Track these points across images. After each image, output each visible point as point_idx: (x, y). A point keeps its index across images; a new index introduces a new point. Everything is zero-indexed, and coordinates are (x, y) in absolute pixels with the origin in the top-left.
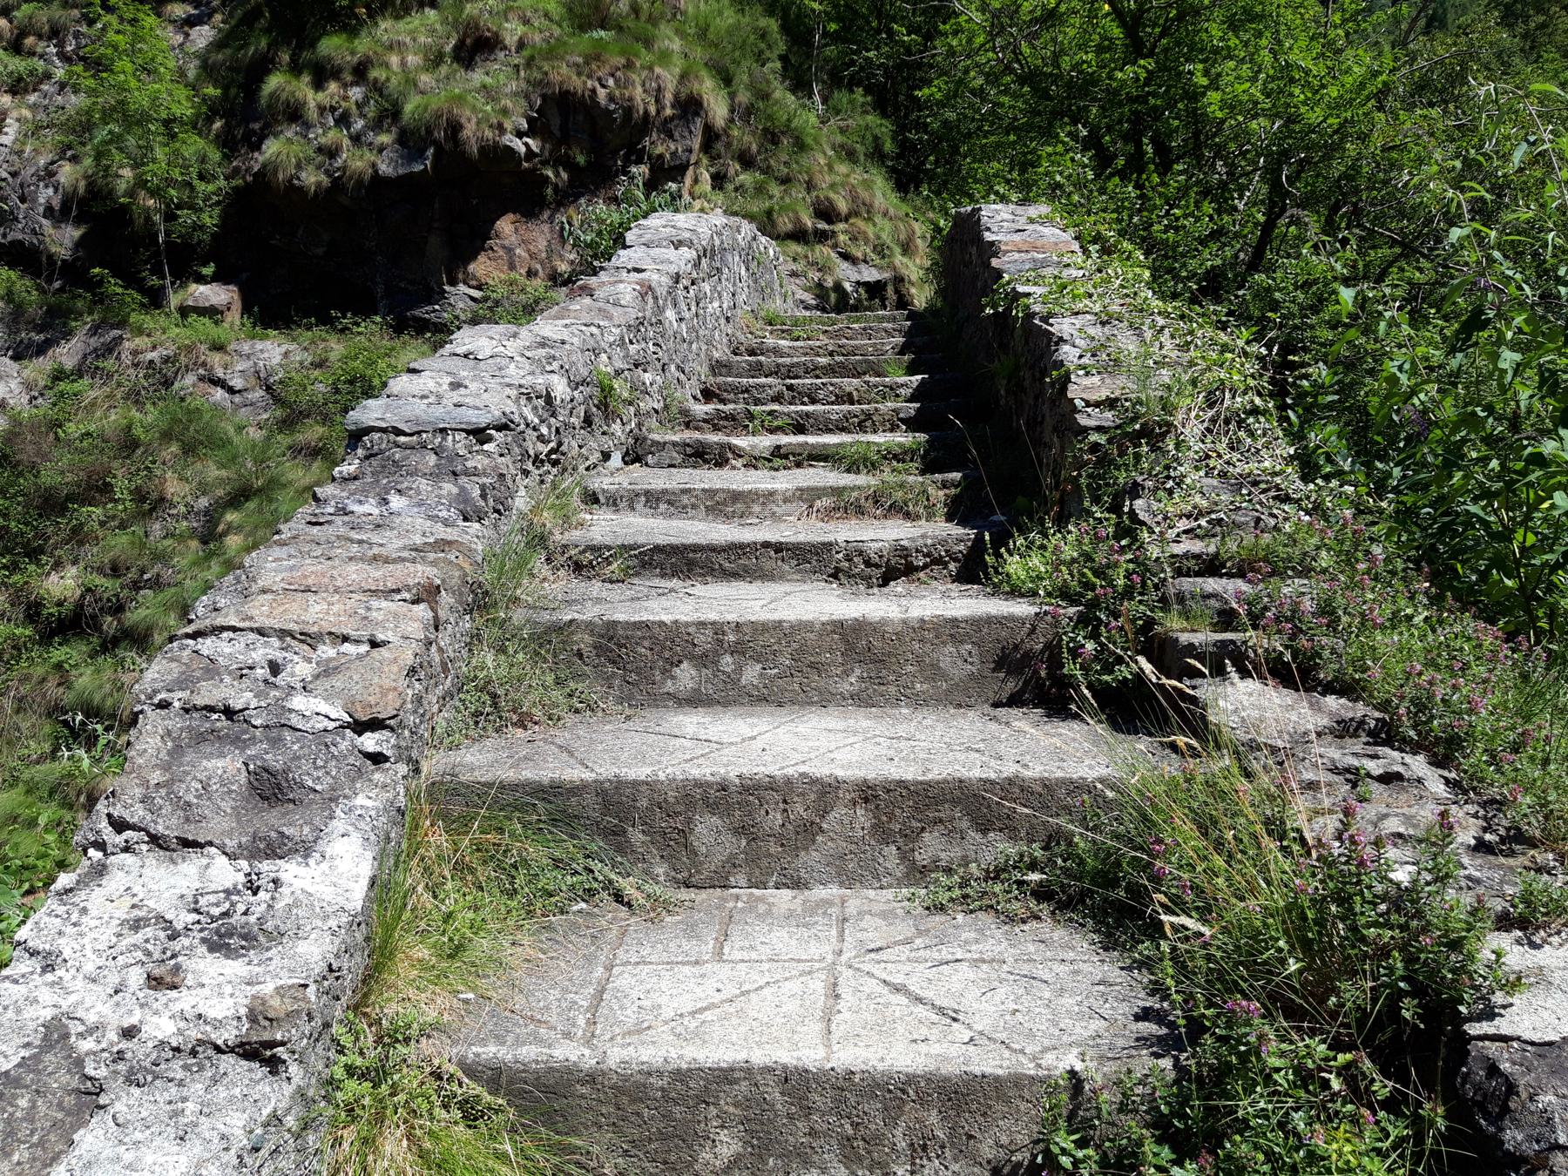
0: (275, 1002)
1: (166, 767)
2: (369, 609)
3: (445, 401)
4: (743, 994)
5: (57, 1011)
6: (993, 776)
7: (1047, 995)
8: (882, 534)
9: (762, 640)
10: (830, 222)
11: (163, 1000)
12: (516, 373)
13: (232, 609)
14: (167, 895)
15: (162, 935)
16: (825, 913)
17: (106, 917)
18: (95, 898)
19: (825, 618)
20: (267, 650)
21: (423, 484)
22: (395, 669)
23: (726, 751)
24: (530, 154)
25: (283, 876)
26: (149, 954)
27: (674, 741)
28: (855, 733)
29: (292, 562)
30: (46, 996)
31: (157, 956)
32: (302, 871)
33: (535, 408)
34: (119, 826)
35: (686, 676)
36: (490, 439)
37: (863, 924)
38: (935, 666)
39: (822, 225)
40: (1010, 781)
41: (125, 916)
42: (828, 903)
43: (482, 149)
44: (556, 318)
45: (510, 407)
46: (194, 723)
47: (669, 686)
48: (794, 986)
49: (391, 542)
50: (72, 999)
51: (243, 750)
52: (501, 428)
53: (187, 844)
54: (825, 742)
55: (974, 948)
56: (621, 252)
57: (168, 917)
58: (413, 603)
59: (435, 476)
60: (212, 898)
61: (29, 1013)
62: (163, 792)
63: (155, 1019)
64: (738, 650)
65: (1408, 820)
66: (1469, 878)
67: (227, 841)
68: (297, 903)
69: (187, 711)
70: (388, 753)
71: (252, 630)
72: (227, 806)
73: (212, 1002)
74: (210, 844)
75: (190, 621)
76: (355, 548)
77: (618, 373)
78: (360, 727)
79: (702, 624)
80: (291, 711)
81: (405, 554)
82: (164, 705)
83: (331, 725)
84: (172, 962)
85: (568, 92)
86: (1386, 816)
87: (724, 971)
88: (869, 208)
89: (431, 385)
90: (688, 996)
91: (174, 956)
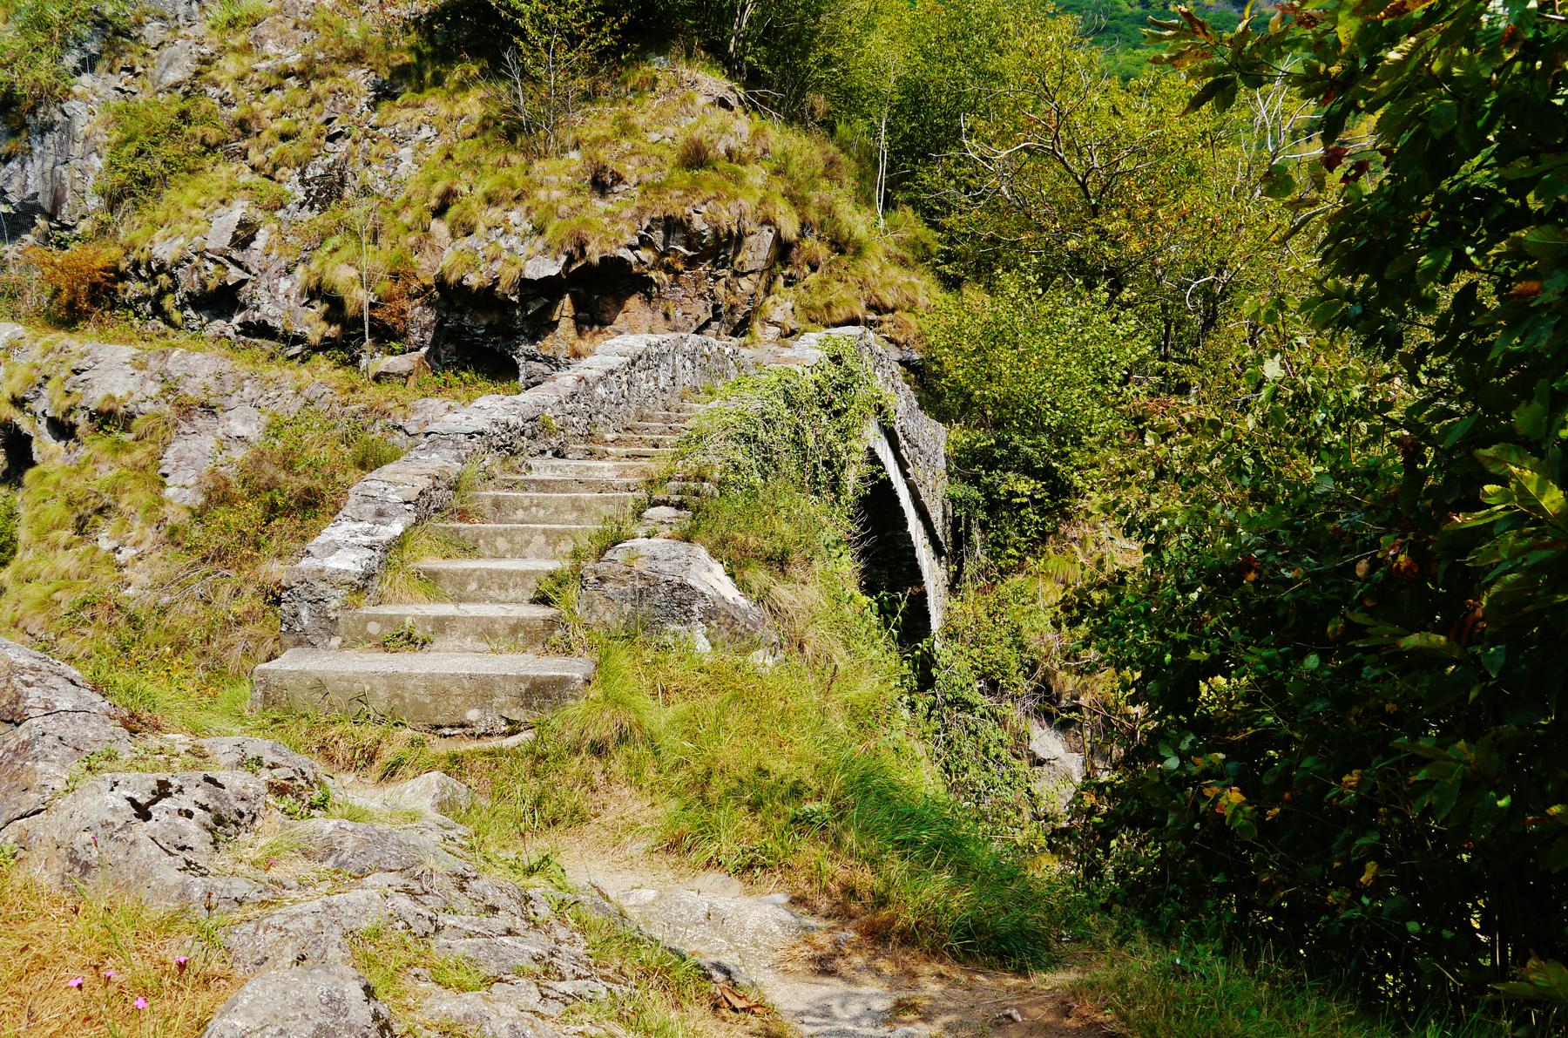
10: (879, 313)
20: (386, 485)
24: (641, 262)
35: (520, 514)
39: (872, 316)
43: (602, 259)
52: (481, 434)
64: (538, 505)
77: (556, 417)
78: (406, 503)
85: (670, 217)
88: (913, 303)
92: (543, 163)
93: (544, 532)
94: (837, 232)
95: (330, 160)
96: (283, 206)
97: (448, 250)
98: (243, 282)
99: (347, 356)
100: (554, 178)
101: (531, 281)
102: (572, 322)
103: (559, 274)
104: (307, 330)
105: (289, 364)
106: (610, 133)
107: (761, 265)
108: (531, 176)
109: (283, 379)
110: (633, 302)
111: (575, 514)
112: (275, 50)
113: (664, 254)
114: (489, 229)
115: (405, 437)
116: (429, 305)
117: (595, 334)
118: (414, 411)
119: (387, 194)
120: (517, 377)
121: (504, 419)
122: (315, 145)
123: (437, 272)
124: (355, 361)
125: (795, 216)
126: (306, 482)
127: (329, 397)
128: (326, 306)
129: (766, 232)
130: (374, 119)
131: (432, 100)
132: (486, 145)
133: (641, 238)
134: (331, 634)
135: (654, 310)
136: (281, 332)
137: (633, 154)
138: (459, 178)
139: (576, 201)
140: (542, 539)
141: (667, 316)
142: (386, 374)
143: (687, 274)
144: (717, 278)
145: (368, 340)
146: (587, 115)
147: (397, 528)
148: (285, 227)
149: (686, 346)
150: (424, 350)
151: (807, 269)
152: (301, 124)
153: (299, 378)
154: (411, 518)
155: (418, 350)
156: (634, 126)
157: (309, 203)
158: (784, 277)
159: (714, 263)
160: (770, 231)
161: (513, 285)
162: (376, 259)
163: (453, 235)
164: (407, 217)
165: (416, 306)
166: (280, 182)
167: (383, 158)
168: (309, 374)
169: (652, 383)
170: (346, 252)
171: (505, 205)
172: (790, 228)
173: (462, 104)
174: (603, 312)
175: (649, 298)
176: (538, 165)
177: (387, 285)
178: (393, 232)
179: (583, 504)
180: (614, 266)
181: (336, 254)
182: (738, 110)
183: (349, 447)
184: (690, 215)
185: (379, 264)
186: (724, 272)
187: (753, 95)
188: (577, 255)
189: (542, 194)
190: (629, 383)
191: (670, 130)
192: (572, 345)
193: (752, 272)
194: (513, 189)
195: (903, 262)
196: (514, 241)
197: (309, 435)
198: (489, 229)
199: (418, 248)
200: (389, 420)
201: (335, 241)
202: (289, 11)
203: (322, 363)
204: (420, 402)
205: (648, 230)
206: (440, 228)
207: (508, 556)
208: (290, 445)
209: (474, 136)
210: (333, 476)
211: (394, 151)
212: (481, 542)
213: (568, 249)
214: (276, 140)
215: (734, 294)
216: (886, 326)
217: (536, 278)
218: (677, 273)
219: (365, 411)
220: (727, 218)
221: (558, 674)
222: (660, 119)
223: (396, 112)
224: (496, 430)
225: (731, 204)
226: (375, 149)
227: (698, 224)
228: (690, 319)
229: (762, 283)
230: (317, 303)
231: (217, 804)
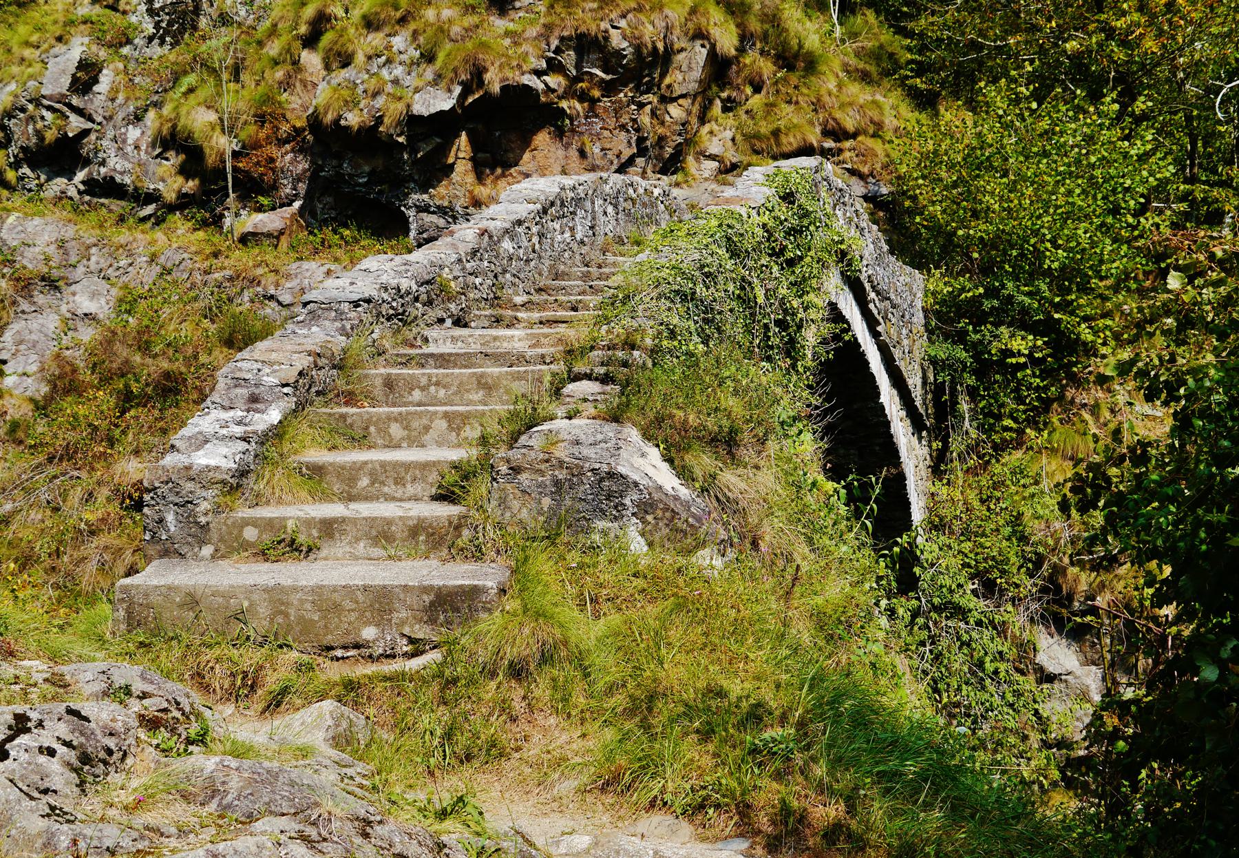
10: (837, 140)
20: (259, 365)
24: (549, 90)
34: (213, 403)
35: (417, 395)
36: (359, 306)
39: (829, 144)
43: (502, 88)
47: (410, 399)
52: (368, 301)
64: (437, 384)
77: (456, 278)
88: (879, 126)
93: (446, 415)
94: (785, 44)
96: (129, 41)
97: (322, 86)
98: (85, 133)
99: (208, 215)
101: (421, 117)
102: (469, 165)
103: (453, 108)
104: (161, 186)
107: (693, 87)
109: (135, 245)
110: (542, 139)
111: (481, 393)
114: (370, 58)
115: (278, 308)
116: (302, 151)
117: (498, 178)
118: (288, 276)
119: (250, 22)
120: (406, 232)
121: (394, 282)
123: (310, 111)
124: (217, 221)
125: (733, 27)
126: (165, 365)
128: (182, 157)
129: (698, 48)
133: (549, 61)
134: (202, 542)
135: (567, 146)
136: (131, 189)
140: (443, 424)
141: (582, 154)
142: (254, 234)
143: (606, 102)
144: (641, 106)
145: (232, 195)
147: (274, 415)
149: (607, 189)
151: (749, 90)
153: (152, 243)
154: (290, 403)
155: (290, 205)
157: (159, 36)
158: (722, 101)
159: (637, 89)
160: (703, 46)
161: (399, 123)
163: (328, 67)
165: (287, 153)
166: (125, 13)
168: (164, 238)
169: (567, 235)
170: (204, 93)
171: (387, 30)
172: (727, 40)
174: (506, 151)
175: (559, 134)
177: (252, 129)
178: (258, 66)
180: (517, 95)
181: (192, 96)
183: (213, 321)
184: (606, 31)
185: (242, 105)
186: (651, 98)
190: (541, 235)
193: (683, 96)
194: (397, 9)
195: (865, 77)
196: (399, 71)
197: (167, 310)
198: (370, 58)
199: (286, 85)
200: (259, 289)
204: (295, 266)
205: (558, 51)
206: (312, 60)
208: (146, 322)
210: (196, 357)
212: (372, 429)
215: (662, 123)
216: (847, 155)
217: (426, 114)
218: (593, 102)
219: (231, 279)
220: (650, 32)
221: (467, 582)
224: (385, 296)
225: (655, 16)
227: (617, 41)
228: (610, 155)
229: (696, 109)
230: (171, 154)
231: (83, 740)
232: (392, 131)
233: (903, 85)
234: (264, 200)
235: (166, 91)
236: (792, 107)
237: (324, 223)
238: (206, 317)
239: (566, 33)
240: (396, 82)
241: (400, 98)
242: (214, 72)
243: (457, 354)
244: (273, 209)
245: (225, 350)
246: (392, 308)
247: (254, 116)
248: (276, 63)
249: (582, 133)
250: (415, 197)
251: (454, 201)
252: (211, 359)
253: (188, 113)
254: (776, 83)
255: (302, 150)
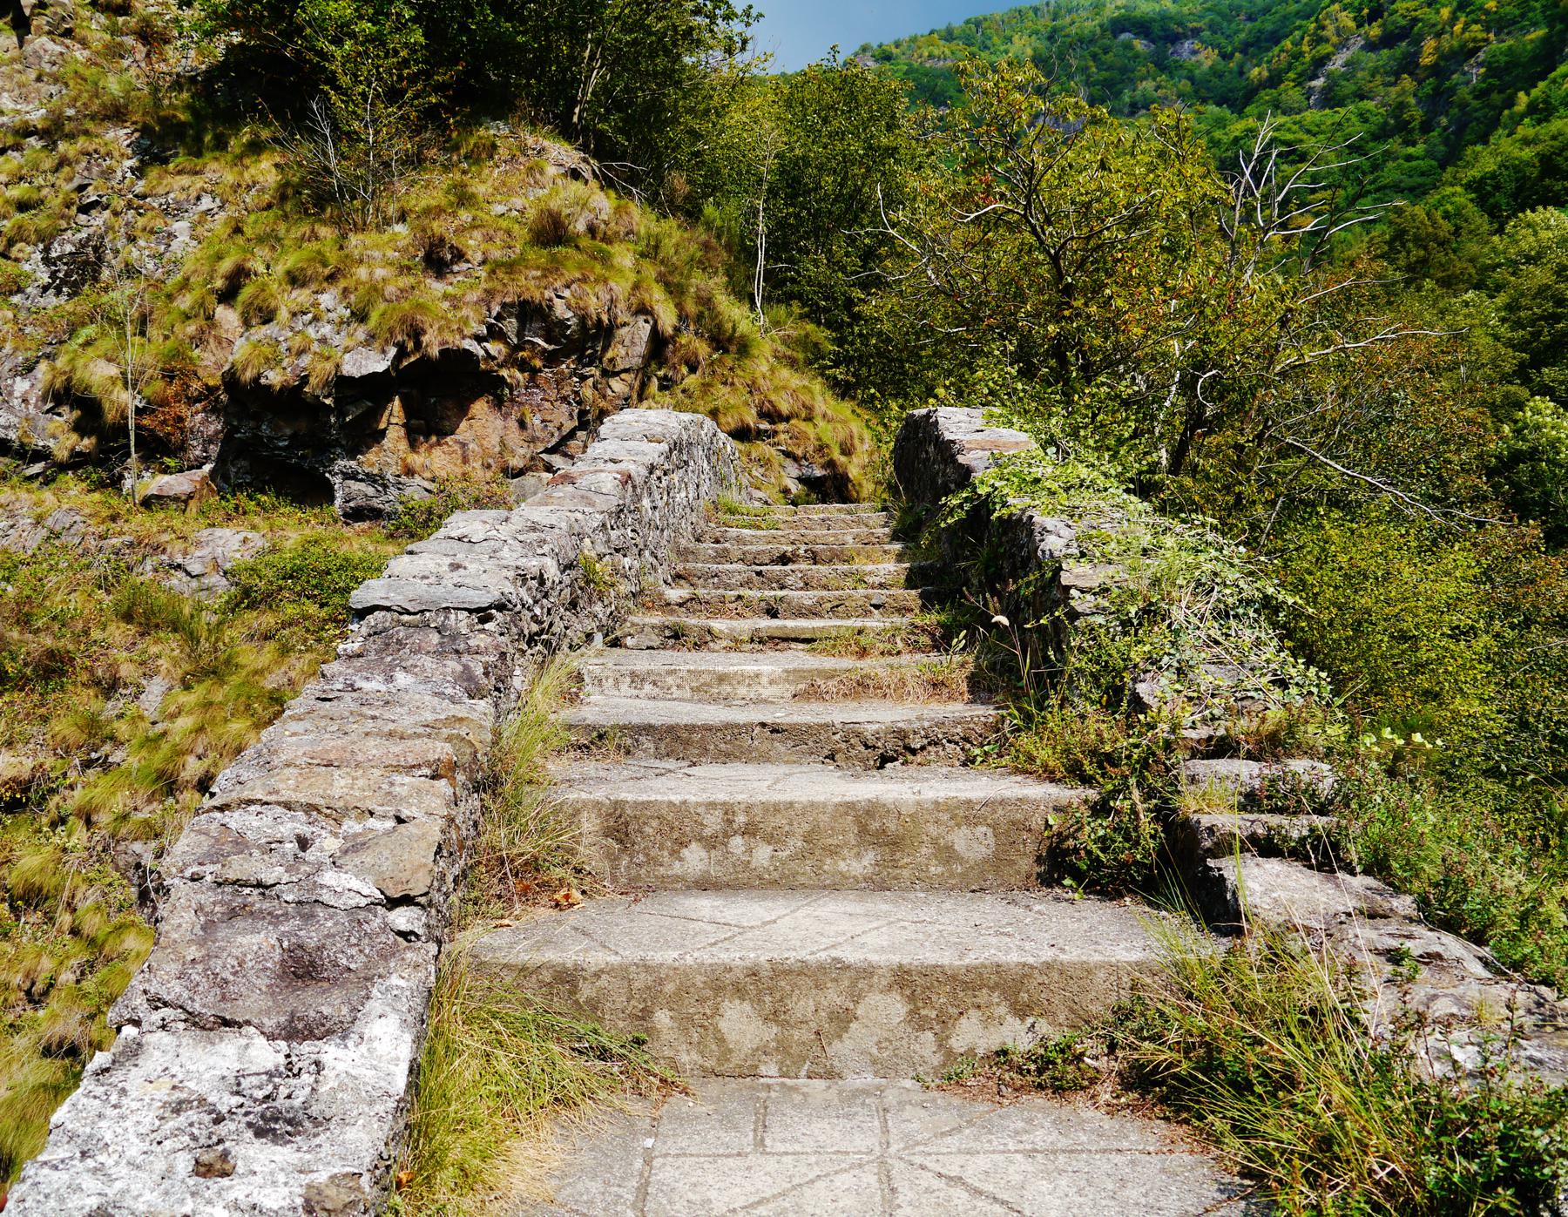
0: (332, 1192)
1: (201, 943)
2: (392, 784)
3: (444, 582)
4: (794, 1188)
5: (103, 1200)
6: (1031, 960)
7: (1110, 1186)
8: (875, 716)
9: (780, 820)
10: (772, 422)
11: (215, 1188)
12: (510, 556)
13: (259, 783)
14: (207, 1076)
15: (207, 1118)
16: (863, 1104)
17: (147, 1099)
18: (133, 1078)
19: (837, 800)
20: (295, 825)
21: (428, 662)
22: (424, 844)
23: (749, 935)
24: (489, 357)
25: (324, 1058)
26: (194, 1138)
27: (692, 925)
28: (878, 917)
29: (312, 736)
30: (90, 1183)
31: (203, 1141)
32: (340, 1053)
33: (529, 589)
34: (156, 1003)
35: (695, 859)
36: (489, 618)
37: (906, 1115)
38: (949, 848)
39: (765, 426)
40: (1048, 966)
41: (166, 1098)
42: (865, 1092)
43: (441, 352)
44: (540, 504)
45: (508, 588)
46: (227, 898)
47: (677, 868)
48: (843, 1181)
49: (406, 722)
50: (118, 1185)
51: (276, 925)
52: (501, 607)
53: (227, 1023)
54: (846, 926)
55: (1024, 1138)
56: (596, 444)
57: (211, 1099)
58: (433, 778)
59: (440, 654)
60: (255, 1080)
61: (74, 1202)
62: (200, 968)
63: (209, 1209)
64: (749, 831)
65: (1458, 1000)
66: (1530, 1058)
67: (265, 1020)
68: (342, 1087)
69: (220, 885)
70: (420, 931)
71: (279, 803)
72: (263, 983)
73: (266, 1191)
74: (248, 1023)
75: (212, 795)
76: (370, 724)
77: (601, 557)
78: (393, 903)
79: (712, 805)
80: (322, 886)
81: (420, 730)
82: (195, 878)
83: (363, 902)
84: (220, 1148)
86: (1435, 997)
87: (771, 1164)
88: (810, 409)
89: (431, 566)
90: (738, 1190)
91: (220, 1141)
92: (360, 236)
94: (719, 326)
95: (83, 235)
96: (20, 290)
97: (239, 342)
99: (104, 475)
100: (376, 254)
101: (351, 379)
102: (402, 432)
103: (387, 371)
104: (51, 443)
105: (26, 485)
106: (444, 202)
107: (637, 362)
108: (346, 251)
109: (17, 505)
110: (480, 407)
111: (869, 857)
112: (11, 105)
113: (519, 348)
114: (294, 314)
115: (186, 579)
116: (214, 411)
117: (432, 446)
118: (198, 544)
119: (158, 274)
120: (331, 500)
122: (63, 217)
123: (226, 368)
124: (115, 483)
125: (672, 305)
126: (48, 642)
127: (81, 528)
128: (77, 413)
129: (641, 323)
130: (140, 187)
131: (214, 165)
132: (286, 217)
133: (490, 327)
135: (506, 417)
136: (16, 445)
137: (476, 227)
138: (253, 253)
139: (406, 281)
140: (895, 1007)
141: (522, 424)
142: (159, 497)
143: (547, 373)
144: (583, 378)
145: (134, 455)
146: (413, 183)
148: (22, 315)
150: (207, 468)
151: (684, 370)
152: (45, 192)
153: (38, 504)
155: (200, 467)
156: (473, 196)
157: (55, 286)
158: (659, 379)
159: (579, 361)
160: (646, 321)
161: (327, 383)
162: (143, 353)
163: (247, 324)
164: (185, 302)
165: (197, 413)
166: (17, 260)
167: (152, 232)
168: (53, 498)
170: (105, 345)
171: (314, 287)
172: (667, 318)
173: (252, 171)
174: (442, 418)
175: (498, 403)
176: (354, 239)
177: (158, 385)
178: (167, 319)
179: (892, 826)
180: (456, 359)
181: (90, 349)
182: (593, 184)
183: (108, 592)
184: (550, 300)
185: (149, 360)
186: (593, 370)
187: (609, 168)
188: (410, 345)
189: (362, 272)
191: (518, 202)
192: (403, 460)
193: (626, 371)
194: (325, 265)
195: (792, 363)
196: (326, 330)
197: (53, 578)
198: (294, 314)
199: (199, 340)
200: (164, 557)
201: (90, 331)
202: (31, 60)
203: (71, 485)
204: (205, 533)
205: (499, 317)
206: (228, 317)
207: (770, 1069)
208: (27, 592)
209: (269, 206)
210: (86, 632)
211: (166, 224)
212: (662, 1018)
213: (400, 338)
214: (11, 210)
215: (604, 397)
216: (782, 437)
217: (357, 375)
218: (534, 372)
219: (131, 545)
220: (595, 305)
222: (503, 189)
223: (169, 179)
225: (599, 288)
226: (141, 222)
227: (561, 310)
228: (551, 427)
229: (637, 384)
230: (65, 409)
232: (318, 392)
233: (822, 375)
234: (171, 462)
235: (61, 342)
236: (728, 389)
237: (237, 488)
238: (100, 587)
239: (508, 300)
240: (323, 341)
241: (328, 358)
242: (120, 325)
243: (708, 728)
244: (181, 471)
245: (123, 625)
246: (535, 619)
247: (163, 369)
248: (187, 317)
249: (521, 404)
250: (342, 464)
251: (385, 469)
252: (105, 635)
253: (86, 366)
254: (712, 364)
255: (215, 409)
